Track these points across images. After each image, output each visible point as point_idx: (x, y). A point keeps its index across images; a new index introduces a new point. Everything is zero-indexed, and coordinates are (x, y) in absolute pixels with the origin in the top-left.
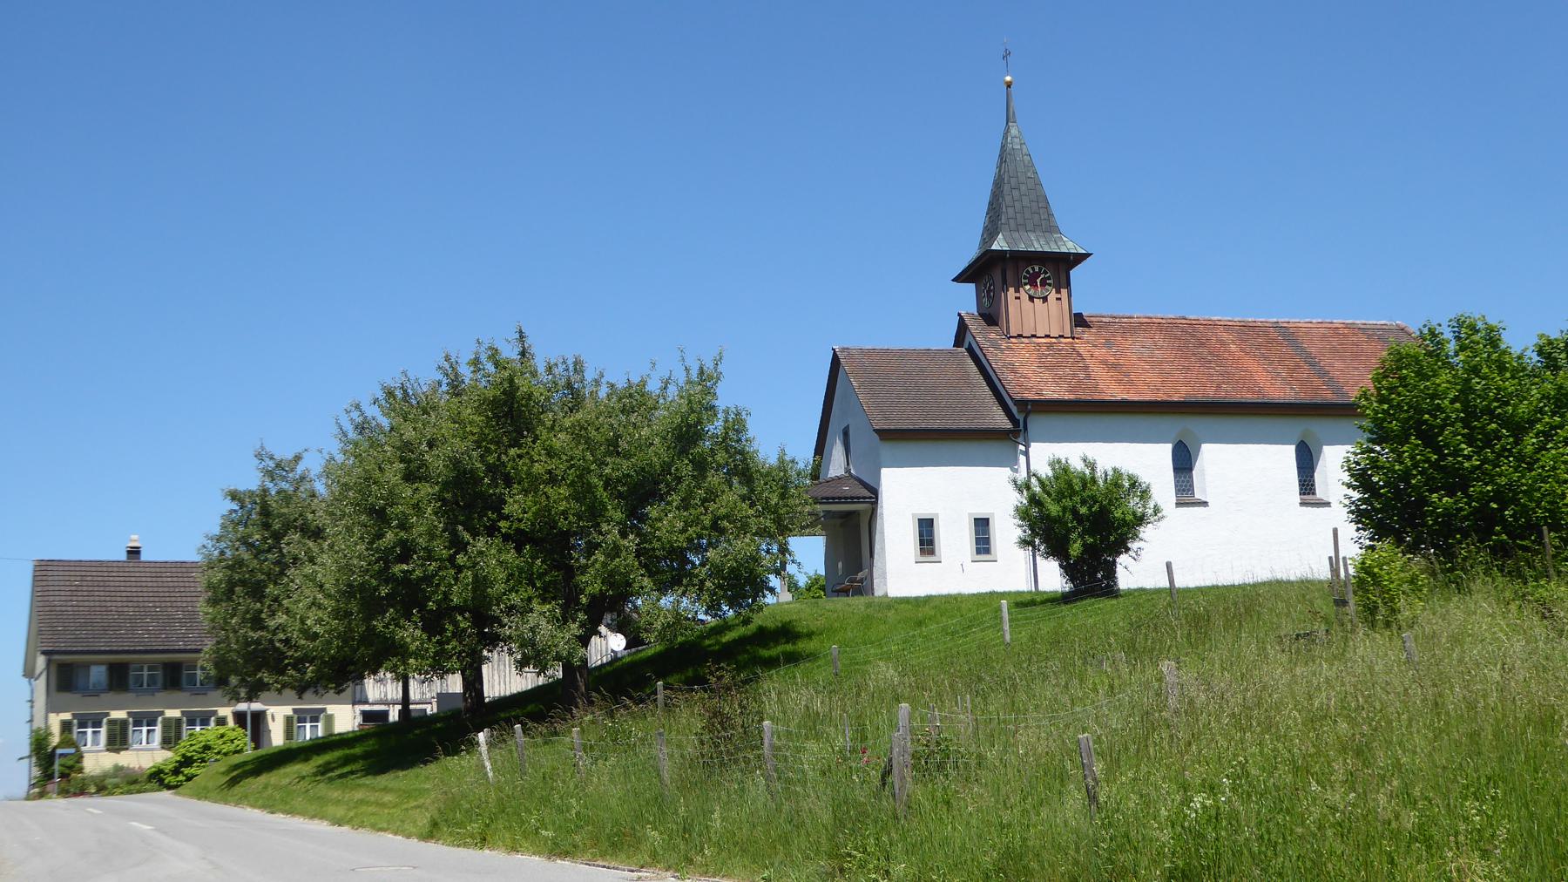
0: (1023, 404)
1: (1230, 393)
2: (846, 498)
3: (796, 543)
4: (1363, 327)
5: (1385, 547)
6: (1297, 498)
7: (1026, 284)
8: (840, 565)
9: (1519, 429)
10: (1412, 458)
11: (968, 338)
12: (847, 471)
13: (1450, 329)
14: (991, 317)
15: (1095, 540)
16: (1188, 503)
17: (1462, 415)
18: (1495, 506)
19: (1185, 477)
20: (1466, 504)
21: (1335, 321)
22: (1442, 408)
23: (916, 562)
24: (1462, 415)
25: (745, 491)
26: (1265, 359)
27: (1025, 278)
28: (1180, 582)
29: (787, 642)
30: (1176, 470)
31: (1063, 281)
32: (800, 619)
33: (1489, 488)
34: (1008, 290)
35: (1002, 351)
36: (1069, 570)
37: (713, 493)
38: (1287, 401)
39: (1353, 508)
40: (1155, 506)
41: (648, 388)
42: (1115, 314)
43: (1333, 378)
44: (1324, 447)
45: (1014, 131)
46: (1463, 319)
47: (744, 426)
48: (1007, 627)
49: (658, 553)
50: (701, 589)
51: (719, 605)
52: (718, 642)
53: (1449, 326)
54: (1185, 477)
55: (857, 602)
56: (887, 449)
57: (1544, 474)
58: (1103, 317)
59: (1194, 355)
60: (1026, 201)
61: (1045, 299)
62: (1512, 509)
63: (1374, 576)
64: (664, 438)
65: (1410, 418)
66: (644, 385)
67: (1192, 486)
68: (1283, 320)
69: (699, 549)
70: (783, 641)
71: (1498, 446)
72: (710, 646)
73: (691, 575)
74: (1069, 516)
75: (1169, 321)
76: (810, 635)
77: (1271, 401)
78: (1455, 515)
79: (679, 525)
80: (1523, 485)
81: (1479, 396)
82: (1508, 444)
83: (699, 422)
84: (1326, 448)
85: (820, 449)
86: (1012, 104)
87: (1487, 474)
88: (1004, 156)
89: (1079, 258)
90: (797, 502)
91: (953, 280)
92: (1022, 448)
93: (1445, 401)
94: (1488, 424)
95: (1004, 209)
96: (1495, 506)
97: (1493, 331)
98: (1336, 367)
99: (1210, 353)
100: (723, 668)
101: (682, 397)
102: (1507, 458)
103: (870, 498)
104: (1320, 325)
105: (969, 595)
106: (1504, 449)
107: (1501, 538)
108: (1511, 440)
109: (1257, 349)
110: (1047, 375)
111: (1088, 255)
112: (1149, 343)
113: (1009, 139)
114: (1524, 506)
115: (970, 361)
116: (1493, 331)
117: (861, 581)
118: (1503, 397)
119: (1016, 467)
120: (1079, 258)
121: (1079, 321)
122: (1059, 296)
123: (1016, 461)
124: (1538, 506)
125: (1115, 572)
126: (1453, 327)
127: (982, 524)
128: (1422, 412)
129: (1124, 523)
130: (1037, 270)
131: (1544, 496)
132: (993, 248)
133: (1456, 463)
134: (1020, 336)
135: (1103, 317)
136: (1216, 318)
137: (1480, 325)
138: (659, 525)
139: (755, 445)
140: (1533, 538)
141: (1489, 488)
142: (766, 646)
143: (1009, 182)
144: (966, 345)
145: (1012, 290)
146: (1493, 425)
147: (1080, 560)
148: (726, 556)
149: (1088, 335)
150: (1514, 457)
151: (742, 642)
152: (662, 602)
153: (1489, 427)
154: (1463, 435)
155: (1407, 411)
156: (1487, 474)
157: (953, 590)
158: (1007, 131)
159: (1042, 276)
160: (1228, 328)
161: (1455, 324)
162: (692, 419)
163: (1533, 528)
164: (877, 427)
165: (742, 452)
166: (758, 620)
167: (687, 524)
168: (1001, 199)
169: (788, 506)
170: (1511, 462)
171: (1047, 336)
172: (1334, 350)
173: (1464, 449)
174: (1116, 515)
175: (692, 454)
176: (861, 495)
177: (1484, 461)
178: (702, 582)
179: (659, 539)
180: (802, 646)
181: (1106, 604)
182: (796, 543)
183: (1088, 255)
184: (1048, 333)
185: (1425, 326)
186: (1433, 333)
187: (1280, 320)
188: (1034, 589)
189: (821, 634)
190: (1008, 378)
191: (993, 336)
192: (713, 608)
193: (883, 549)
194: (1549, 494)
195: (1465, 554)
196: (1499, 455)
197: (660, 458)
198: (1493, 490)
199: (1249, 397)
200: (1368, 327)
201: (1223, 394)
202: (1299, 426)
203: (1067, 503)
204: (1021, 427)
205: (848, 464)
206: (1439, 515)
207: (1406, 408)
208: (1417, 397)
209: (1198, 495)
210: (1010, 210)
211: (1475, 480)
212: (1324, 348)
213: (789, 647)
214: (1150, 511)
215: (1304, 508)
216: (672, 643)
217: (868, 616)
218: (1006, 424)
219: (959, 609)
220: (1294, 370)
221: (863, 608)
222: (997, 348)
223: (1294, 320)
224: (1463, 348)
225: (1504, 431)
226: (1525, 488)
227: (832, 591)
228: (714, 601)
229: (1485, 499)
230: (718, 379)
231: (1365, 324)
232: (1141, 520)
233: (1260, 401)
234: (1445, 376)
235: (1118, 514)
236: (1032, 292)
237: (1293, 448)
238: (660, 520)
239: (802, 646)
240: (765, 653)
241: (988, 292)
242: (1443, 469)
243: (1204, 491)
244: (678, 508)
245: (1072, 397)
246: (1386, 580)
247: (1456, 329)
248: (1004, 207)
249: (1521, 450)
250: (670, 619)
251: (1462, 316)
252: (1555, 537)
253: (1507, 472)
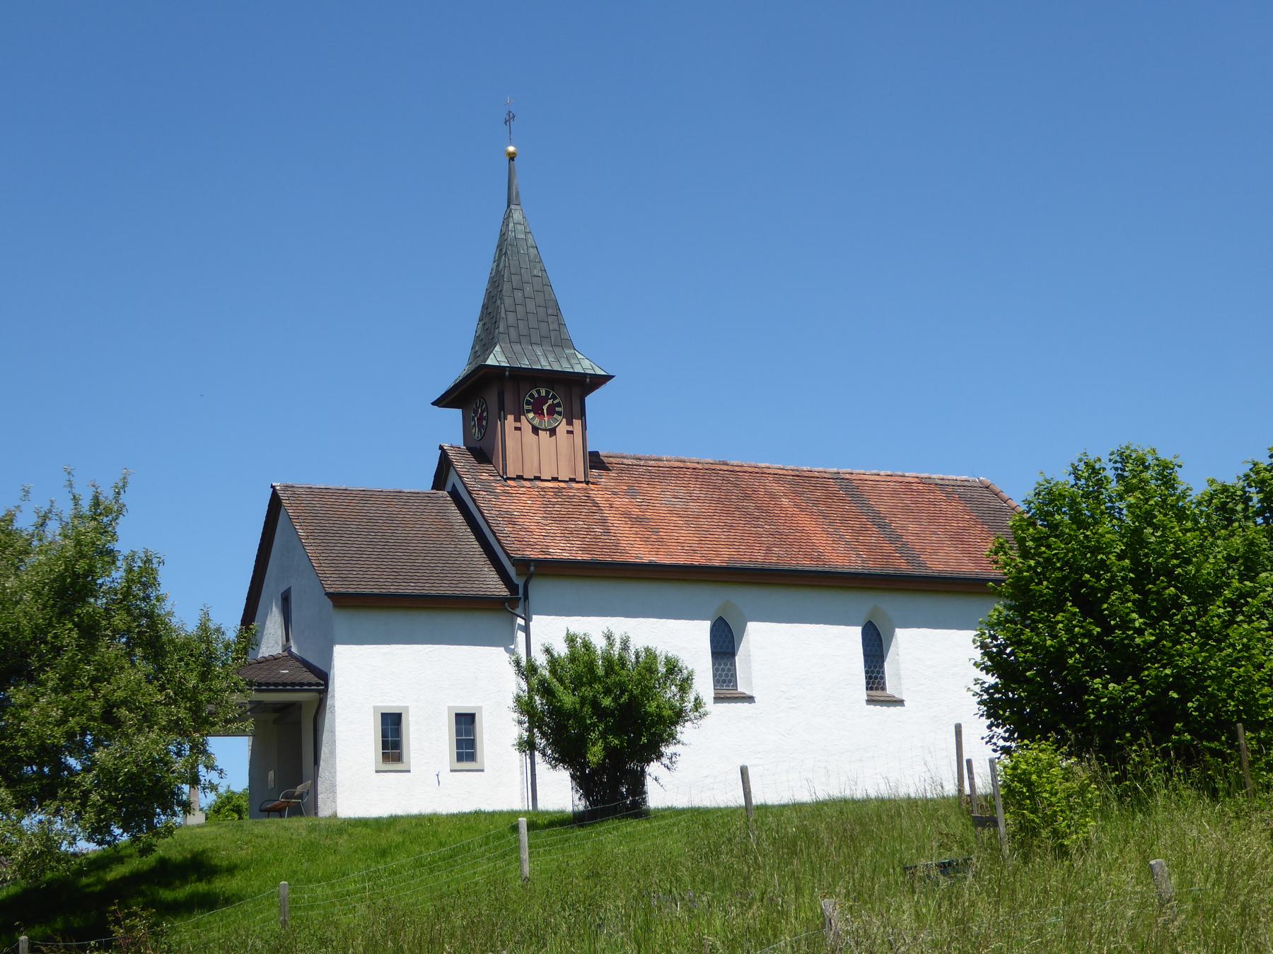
0: (524, 565)
1: (781, 557)
2: (285, 684)
3: (216, 745)
4: (940, 482)
5: (1040, 752)
6: (863, 694)
7: (529, 411)
8: (271, 774)
9: (1204, 595)
10: (1069, 630)
11: (452, 479)
12: (287, 648)
13: (1111, 464)
14: (482, 452)
15: (622, 742)
16: (730, 698)
17: (1132, 575)
18: (1175, 696)
19: (725, 665)
20: (1138, 692)
21: (907, 474)
22: (1108, 566)
23: (377, 772)
24: (1132, 575)
25: (150, 668)
26: (825, 517)
27: (528, 403)
28: (757, 799)
29: (200, 880)
30: (715, 654)
31: (576, 406)
32: (218, 848)
33: (1168, 671)
34: (505, 418)
35: (497, 496)
36: (584, 782)
37: (106, 669)
38: (853, 571)
39: (985, 697)
40: (696, 699)
41: (17, 525)
42: (639, 455)
43: (905, 544)
44: (898, 631)
45: (517, 216)
46: (1128, 452)
47: (154, 578)
48: (525, 855)
49: (22, 753)
50: (83, 805)
51: (108, 826)
52: (100, 881)
53: (1110, 460)
54: (725, 665)
55: (297, 825)
56: (342, 620)
57: (1235, 655)
58: (622, 457)
59: (737, 508)
60: (531, 306)
61: (553, 432)
62: (1197, 700)
63: (1030, 785)
64: (38, 594)
65: (1065, 578)
66: (11, 521)
67: (734, 675)
68: (844, 470)
69: (78, 748)
70: (194, 877)
71: (1179, 617)
72: (88, 885)
73: (70, 784)
74: (587, 710)
75: (706, 466)
76: (231, 870)
77: (833, 570)
78: (1124, 707)
79: (56, 713)
80: (1211, 668)
81: (1153, 551)
82: (1190, 614)
83: (91, 571)
84: (899, 632)
85: (250, 615)
86: (516, 182)
87: (1165, 654)
88: (504, 247)
89: (597, 381)
90: (225, 684)
91: (433, 404)
92: (520, 621)
93: (1110, 556)
94: (1165, 588)
95: (503, 315)
96: (1175, 696)
97: (1167, 467)
98: (910, 529)
99: (757, 508)
100: (135, 914)
101: (66, 537)
102: (1188, 632)
103: (318, 684)
104: (889, 479)
105: (447, 815)
106: (1185, 621)
107: (1183, 738)
108: (1194, 609)
109: (815, 505)
110: (554, 528)
111: (607, 378)
112: (682, 492)
113: (511, 225)
114: (1212, 696)
115: (453, 507)
116: (1167, 467)
117: (301, 796)
118: (1183, 552)
119: (512, 647)
120: (597, 381)
121: (595, 461)
122: (570, 428)
123: (512, 639)
124: (1231, 696)
125: (643, 785)
126: (1116, 462)
127: (466, 722)
128: (1079, 570)
129: (661, 719)
130: (543, 394)
131: (1237, 683)
132: (489, 362)
133: (1125, 639)
134: (520, 478)
135: (622, 457)
136: (763, 465)
137: (1150, 460)
138: (26, 713)
139: (167, 606)
140: (1223, 738)
141: (1168, 671)
142: (168, 885)
143: (510, 281)
144: (449, 487)
145: (510, 418)
146: (1171, 588)
147: (601, 768)
148: (122, 757)
149: (605, 479)
150: (1198, 632)
151: (135, 880)
152: (25, 822)
153: (1167, 591)
154: (1134, 602)
155: (1061, 569)
156: (1165, 654)
157: (427, 810)
158: (508, 217)
159: (550, 402)
160: (778, 477)
161: (1118, 459)
162: (81, 566)
163: (1223, 726)
164: (331, 590)
165: (150, 616)
166: (165, 848)
167: (67, 714)
168: (499, 302)
169: (211, 690)
170: (1193, 638)
171: (555, 479)
172: (906, 509)
173: (1135, 620)
174: (649, 710)
175: (78, 615)
176: (305, 681)
177: (1161, 636)
178: (85, 795)
179: (25, 734)
180: (221, 885)
181: (641, 825)
182: (216, 745)
183: (607, 378)
184: (555, 476)
185: (1080, 460)
186: (1095, 471)
187: (841, 471)
188: (531, 808)
189: (247, 868)
190: (504, 529)
191: (485, 476)
192: (98, 831)
193: (333, 753)
194: (1243, 682)
195: (1137, 759)
196: (1179, 629)
197: (31, 619)
198: (1172, 675)
199: (806, 564)
200: (947, 482)
201: (774, 560)
202: (867, 603)
203: (586, 691)
204: (521, 595)
205: (288, 639)
206: (1102, 707)
207: (1058, 565)
208: (1074, 550)
209: (742, 688)
210: (511, 317)
211: (1148, 660)
212: (895, 507)
213: (202, 887)
214: (689, 705)
215: (872, 707)
216: (37, 880)
217: (312, 843)
218: (501, 590)
219: (435, 834)
220: (859, 532)
221: (304, 834)
222: (490, 491)
223: (858, 471)
224: (1129, 489)
225: (1186, 597)
226: (1214, 672)
227: (261, 811)
228: (102, 821)
229: (1163, 685)
230: (120, 512)
231: (943, 479)
232: (679, 716)
233: (820, 569)
234: (1106, 526)
235: (652, 707)
236: (536, 422)
237: (859, 630)
238: (27, 706)
239: (221, 885)
240: (167, 895)
241: (480, 419)
242: (1109, 646)
243: (749, 682)
244: (54, 690)
245: (586, 557)
246: (1046, 791)
247: (1119, 465)
248: (503, 311)
249: (1207, 623)
250: (37, 846)
251: (1128, 448)
252: (1252, 739)
253: (1189, 650)
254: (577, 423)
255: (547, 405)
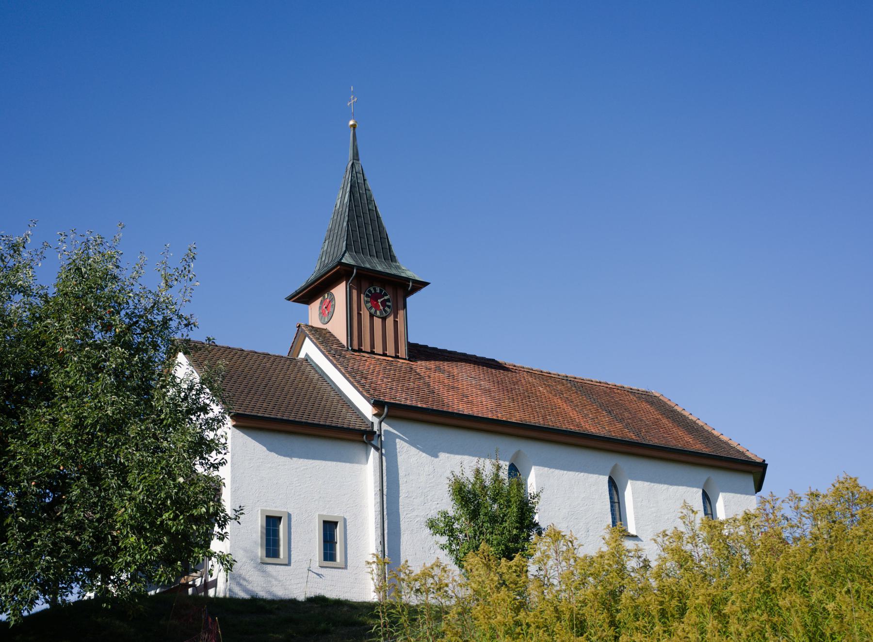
31: (400, 305)
89: (420, 285)
120: (420, 285)
202: (610, 461)
254: (401, 313)
255: (382, 300)
